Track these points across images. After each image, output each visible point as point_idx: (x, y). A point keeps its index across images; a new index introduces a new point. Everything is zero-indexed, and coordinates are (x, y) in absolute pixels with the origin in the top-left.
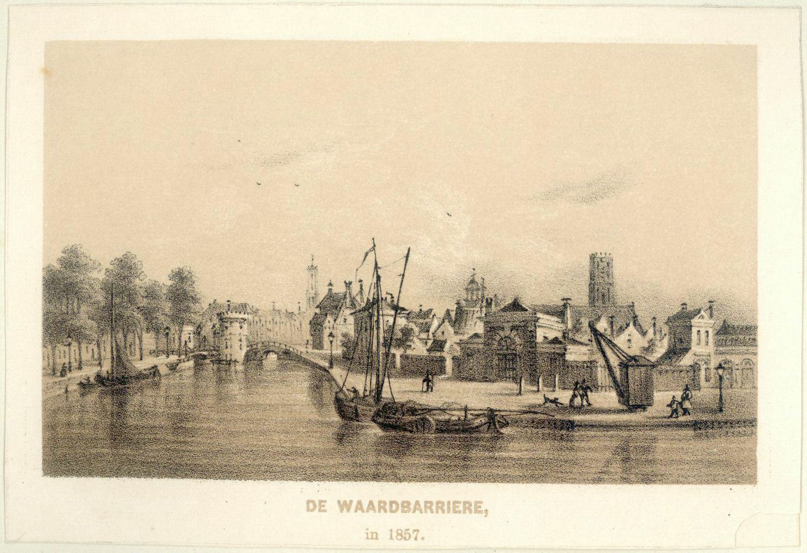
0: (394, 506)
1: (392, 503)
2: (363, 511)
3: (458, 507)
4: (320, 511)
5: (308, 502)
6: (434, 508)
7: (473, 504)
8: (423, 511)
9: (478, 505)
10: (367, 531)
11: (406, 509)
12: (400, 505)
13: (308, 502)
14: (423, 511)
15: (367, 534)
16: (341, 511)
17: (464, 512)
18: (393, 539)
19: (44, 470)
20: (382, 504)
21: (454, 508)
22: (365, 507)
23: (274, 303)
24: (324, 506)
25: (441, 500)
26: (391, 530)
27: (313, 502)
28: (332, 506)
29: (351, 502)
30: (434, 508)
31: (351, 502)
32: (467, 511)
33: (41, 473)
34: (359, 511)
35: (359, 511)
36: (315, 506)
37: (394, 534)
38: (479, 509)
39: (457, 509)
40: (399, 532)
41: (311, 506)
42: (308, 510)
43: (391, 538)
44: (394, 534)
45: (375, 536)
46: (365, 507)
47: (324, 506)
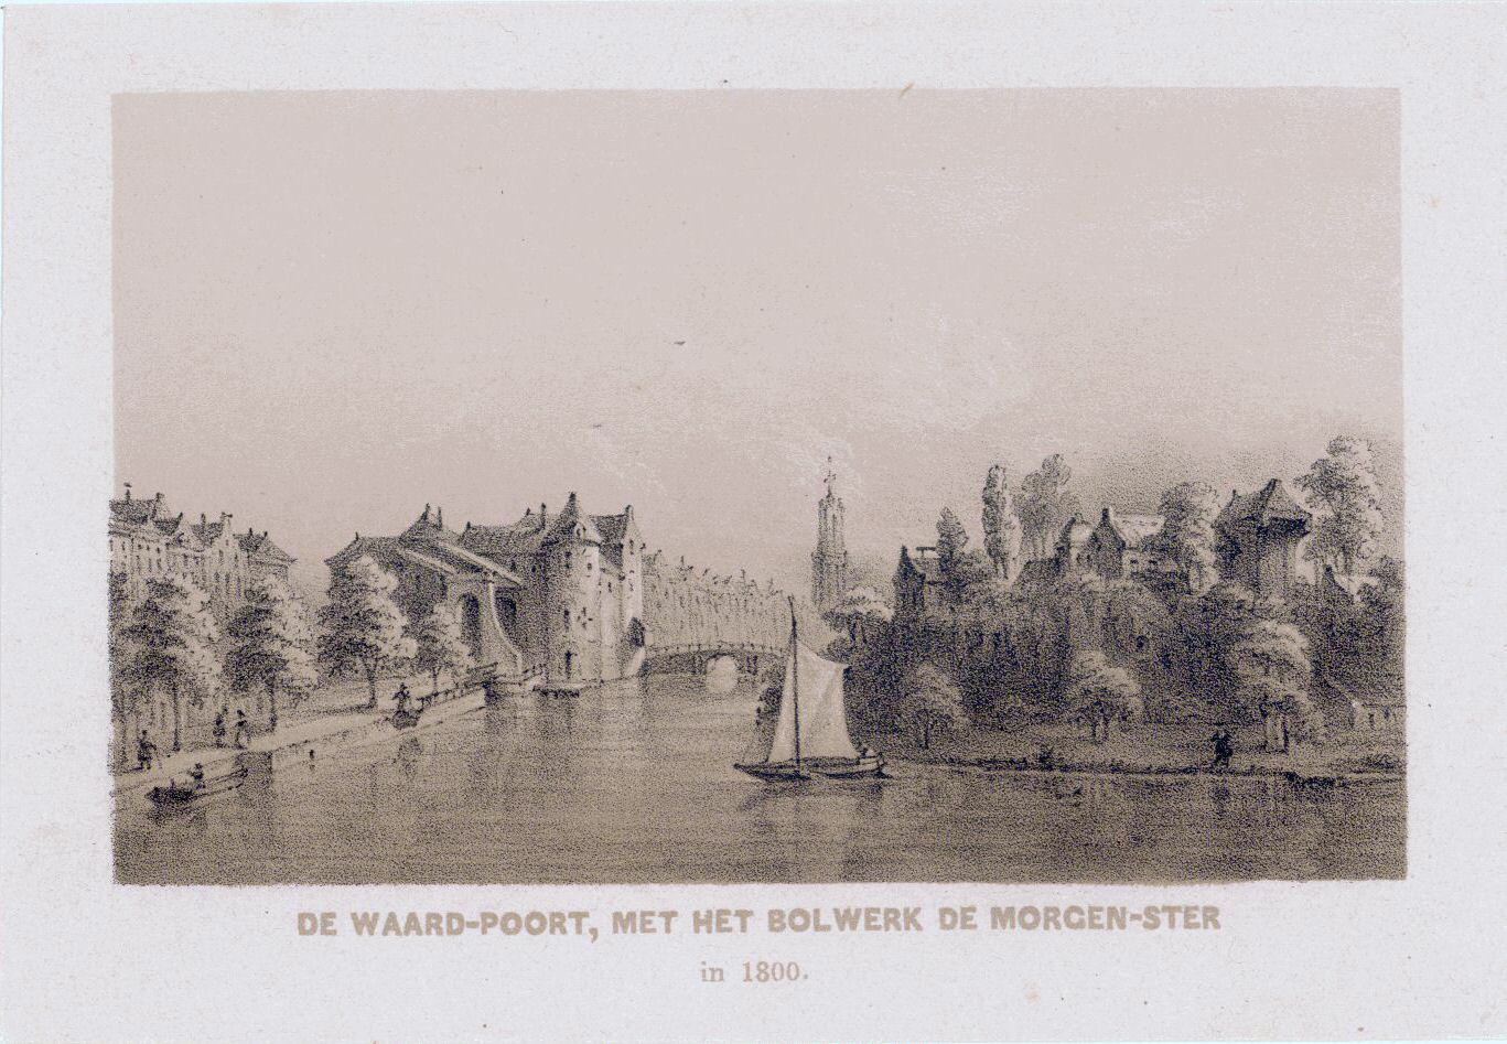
0: (948, 919)
1: (451, 916)
2: (419, 933)
3: (1195, 916)
4: (964, 927)
5: (302, 917)
6: (901, 919)
7: (444, 920)
8: (424, 929)
9: (647, 918)
10: (704, 967)
11: (777, 925)
12: (1042, 916)
13: (302, 917)
14: (424, 929)
15: (704, 971)
16: (842, 929)
17: (1206, 927)
18: (751, 980)
19: (1393, 877)
20: (435, 920)
21: (643, 925)
22: (402, 924)
23: (128, 486)
24: (332, 923)
25: (893, 906)
26: (747, 966)
27: (312, 917)
28: (982, 918)
29: (376, 915)
30: (901, 919)
31: (376, 915)
32: (892, 926)
33: (1398, 883)
34: (392, 934)
35: (392, 934)
36: (543, 924)
37: (754, 973)
38: (873, 923)
39: (1096, 922)
40: (762, 967)
41: (948, 919)
42: (303, 931)
43: (748, 978)
44: (754, 973)
45: (717, 974)
46: (402, 924)
47: (650, 922)
